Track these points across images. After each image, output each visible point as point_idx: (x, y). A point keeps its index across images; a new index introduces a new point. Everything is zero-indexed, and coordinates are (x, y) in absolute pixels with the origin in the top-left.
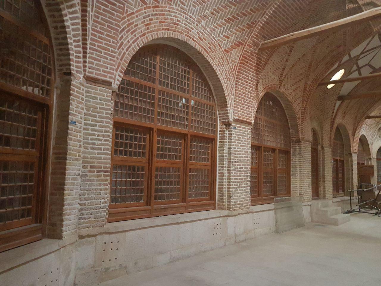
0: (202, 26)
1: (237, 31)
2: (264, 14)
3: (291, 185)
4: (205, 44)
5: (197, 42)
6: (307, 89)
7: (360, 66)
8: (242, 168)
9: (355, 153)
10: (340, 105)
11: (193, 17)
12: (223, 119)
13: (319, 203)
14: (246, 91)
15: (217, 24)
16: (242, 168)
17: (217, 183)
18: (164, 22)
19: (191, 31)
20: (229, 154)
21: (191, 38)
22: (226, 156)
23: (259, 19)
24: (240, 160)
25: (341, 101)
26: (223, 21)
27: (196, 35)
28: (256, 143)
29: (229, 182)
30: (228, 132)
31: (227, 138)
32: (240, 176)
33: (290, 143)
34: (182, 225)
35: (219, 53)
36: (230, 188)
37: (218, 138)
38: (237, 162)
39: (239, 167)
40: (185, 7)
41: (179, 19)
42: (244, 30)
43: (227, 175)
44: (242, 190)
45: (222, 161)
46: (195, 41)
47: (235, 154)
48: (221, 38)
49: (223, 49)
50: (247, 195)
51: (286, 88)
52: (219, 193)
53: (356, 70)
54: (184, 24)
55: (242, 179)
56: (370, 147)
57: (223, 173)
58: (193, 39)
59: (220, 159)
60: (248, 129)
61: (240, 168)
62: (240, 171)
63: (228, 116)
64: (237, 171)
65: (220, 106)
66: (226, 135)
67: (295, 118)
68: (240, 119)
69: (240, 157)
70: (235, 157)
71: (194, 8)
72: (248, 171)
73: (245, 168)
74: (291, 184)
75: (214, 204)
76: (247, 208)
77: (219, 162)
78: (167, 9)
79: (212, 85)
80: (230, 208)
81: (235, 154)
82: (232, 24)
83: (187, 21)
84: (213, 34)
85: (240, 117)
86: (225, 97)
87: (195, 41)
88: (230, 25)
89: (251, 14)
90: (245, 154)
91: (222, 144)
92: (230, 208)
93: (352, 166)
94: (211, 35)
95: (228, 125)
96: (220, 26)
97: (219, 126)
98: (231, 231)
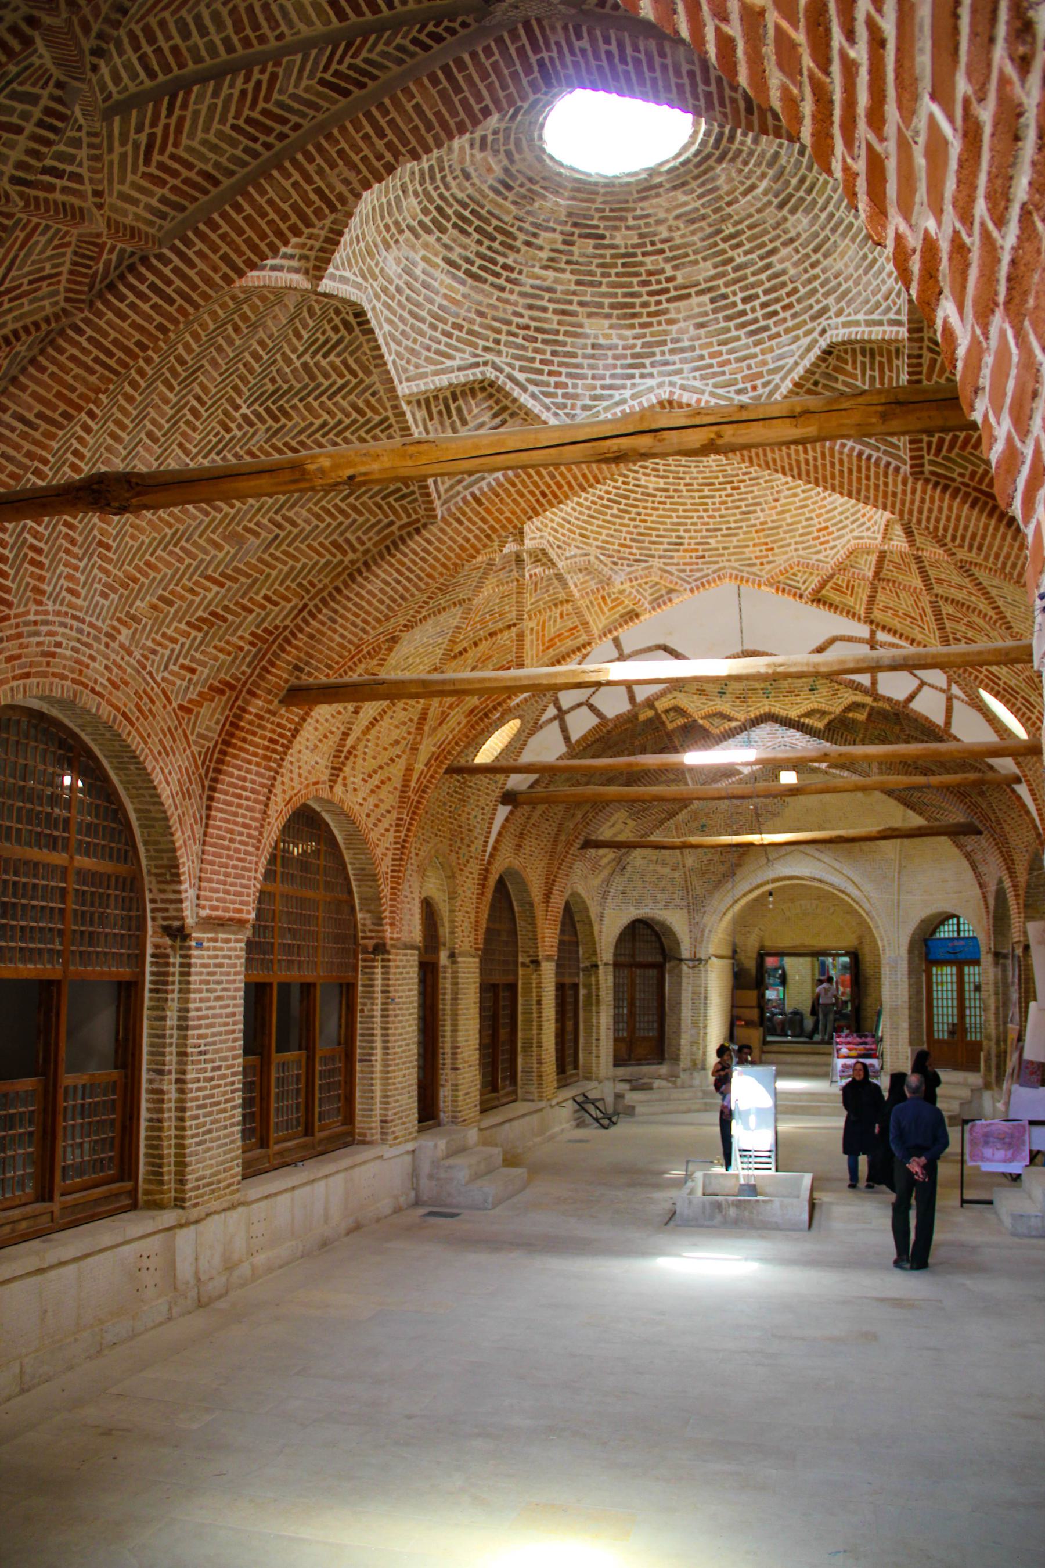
0: (122, 646)
1: (221, 650)
2: (301, 611)
3: (358, 1094)
4: (128, 695)
5: (102, 696)
6: (413, 784)
7: (565, 706)
8: (219, 1068)
9: (549, 958)
10: (507, 820)
11: (99, 624)
12: (164, 919)
13: (435, 1144)
14: (236, 823)
15: (164, 635)
16: (219, 1068)
17: (143, 1124)
18: (19, 657)
19: (87, 666)
20: (180, 1028)
21: (86, 686)
22: (173, 1037)
23: (287, 622)
24: (214, 1043)
25: (509, 808)
26: (183, 626)
27: (102, 675)
28: (260, 976)
29: (182, 1119)
30: (178, 960)
31: (177, 978)
32: (212, 1096)
33: (356, 957)
34: (52, 1274)
35: (164, 718)
36: (183, 1137)
37: (148, 978)
38: (205, 1053)
39: (209, 1066)
40: (79, 602)
41: (58, 639)
42: (241, 649)
43: (174, 1095)
44: (219, 1138)
45: (158, 1052)
46: (98, 694)
47: (199, 1027)
48: (172, 673)
49: (175, 705)
50: (231, 1151)
51: (350, 787)
52: (147, 1155)
53: (554, 718)
54: (73, 649)
55: (218, 1103)
56: (596, 928)
57: (161, 1092)
58: (93, 690)
59: (152, 1045)
60: (237, 941)
61: (214, 1069)
62: (212, 1079)
63: (181, 910)
64: (206, 1080)
65: (156, 875)
66: (171, 969)
67: (374, 878)
68: (215, 913)
69: (214, 1035)
70: (200, 1037)
71: (102, 601)
72: (234, 1074)
73: (228, 1067)
74: (358, 1088)
75: (133, 1193)
76: (232, 1193)
77: (151, 1053)
78: (31, 617)
79: (136, 810)
80: (183, 1200)
81: (199, 1027)
82: (206, 634)
83: (78, 641)
84: (148, 664)
85: (216, 908)
86: (175, 850)
87: (98, 694)
88: (200, 635)
89: (264, 607)
90: (227, 1024)
91: (158, 999)
92: (183, 1200)
93: (539, 1003)
94: (144, 668)
95: (178, 934)
96: (174, 641)
97: (152, 939)
98: (185, 1270)
